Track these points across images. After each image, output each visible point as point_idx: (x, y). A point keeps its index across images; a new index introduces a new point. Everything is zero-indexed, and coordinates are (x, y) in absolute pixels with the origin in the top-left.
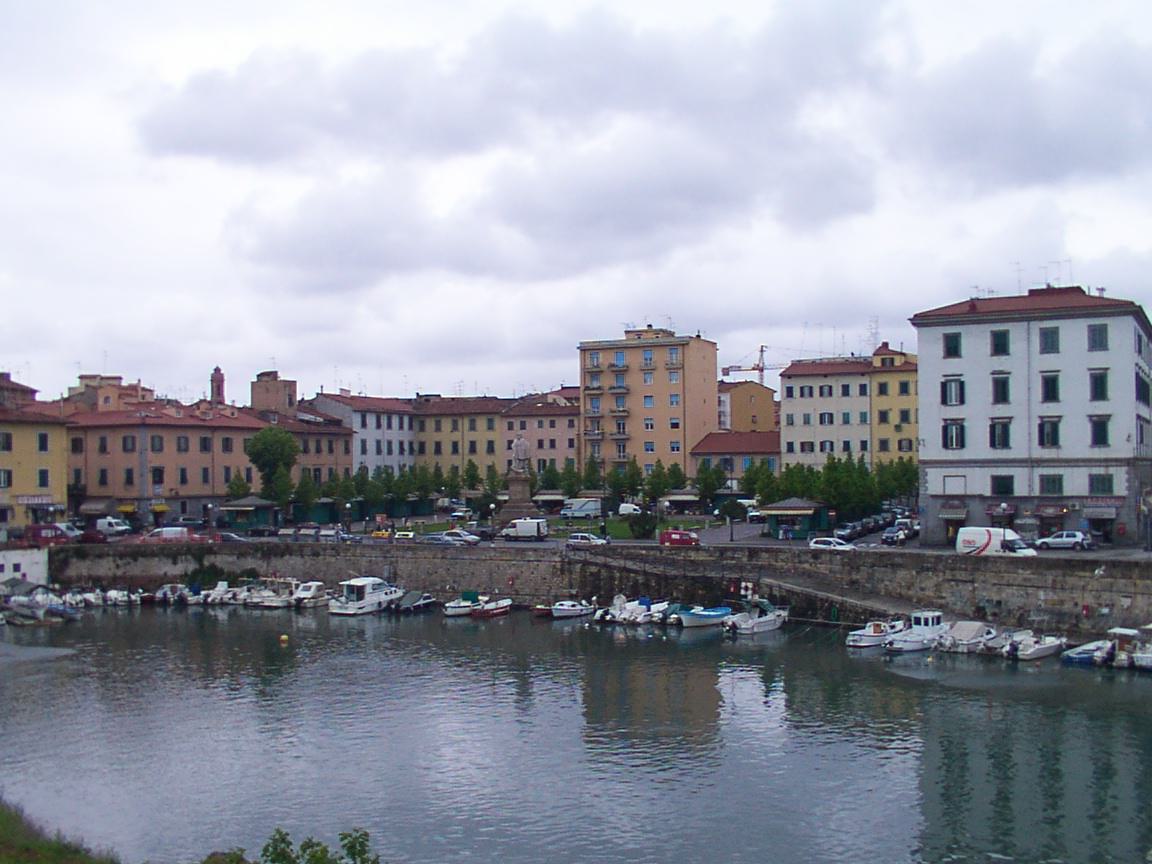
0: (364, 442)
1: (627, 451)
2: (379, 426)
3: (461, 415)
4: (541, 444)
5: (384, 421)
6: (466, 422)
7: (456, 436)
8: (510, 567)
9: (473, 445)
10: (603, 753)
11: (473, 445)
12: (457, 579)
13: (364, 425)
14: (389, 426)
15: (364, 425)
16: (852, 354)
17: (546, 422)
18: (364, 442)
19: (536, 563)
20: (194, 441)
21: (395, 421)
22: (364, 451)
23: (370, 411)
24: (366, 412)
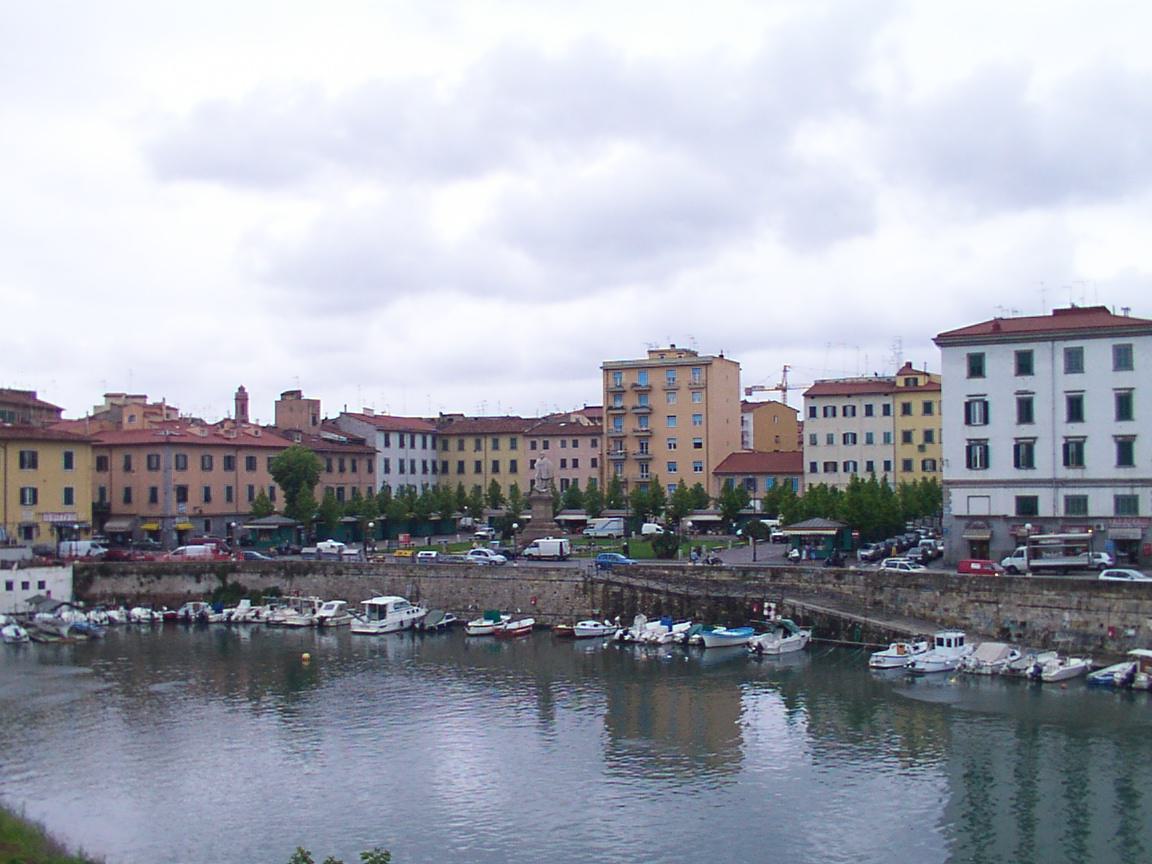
0: (387, 461)
2: (402, 445)
3: (485, 435)
4: (563, 463)
5: (407, 439)
6: (588, 440)
8: (533, 587)
9: (496, 464)
11: (496, 464)
13: (387, 444)
14: (413, 446)
15: (387, 444)
18: (387, 461)
21: (418, 440)
22: (387, 470)
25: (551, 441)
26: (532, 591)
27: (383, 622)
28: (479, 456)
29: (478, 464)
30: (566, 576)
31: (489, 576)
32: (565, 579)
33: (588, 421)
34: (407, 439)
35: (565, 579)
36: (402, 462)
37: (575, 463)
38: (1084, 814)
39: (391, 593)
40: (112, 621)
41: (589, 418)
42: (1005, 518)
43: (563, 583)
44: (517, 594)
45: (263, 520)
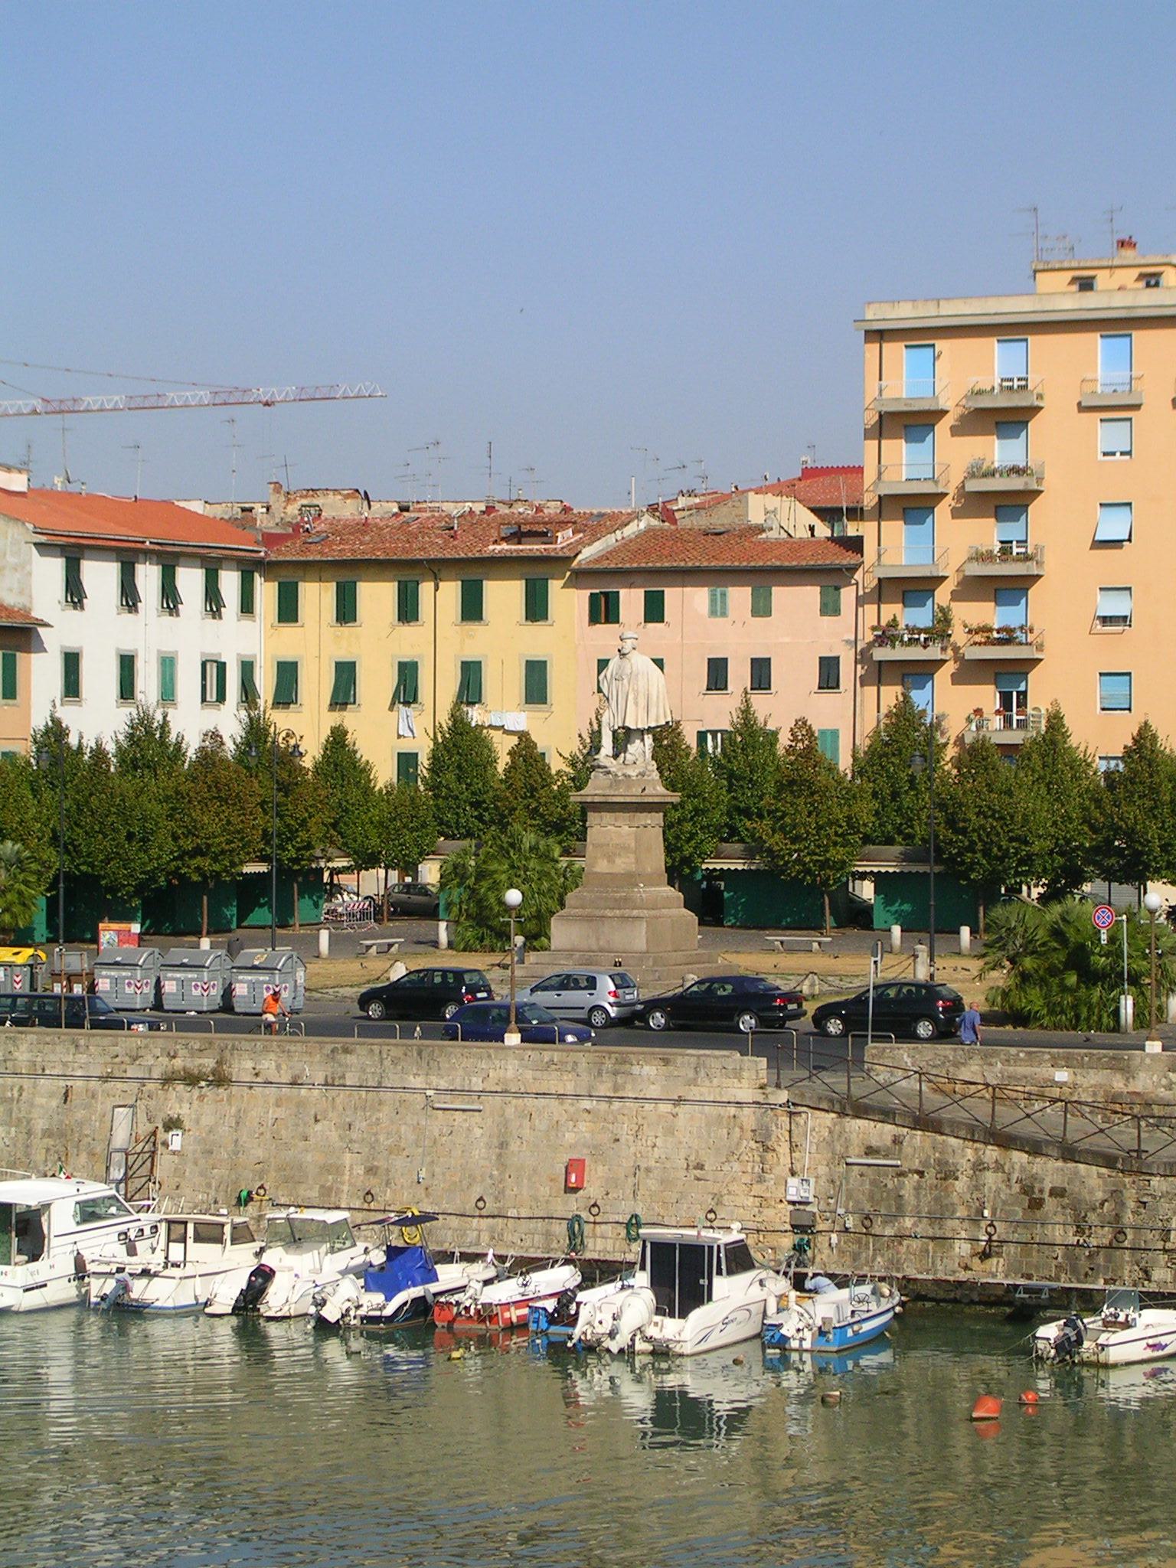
0: (72, 662)
1: (1031, 703)
2: (129, 597)
3: (436, 569)
4: (717, 674)
5: (148, 577)
6: (450, 592)
7: (411, 642)
8: (574, 1120)
9: (346, 675)
10: (15, 1395)
11: (346, 675)
12: (381, 1163)
13: (75, 593)
14: (247, 606)
15: (75, 593)
16: (779, 480)
17: (740, 596)
18: (72, 662)
19: (665, 1108)
20: (632, 600)
21: (190, 580)
22: (72, 688)
23: (148, 555)
24: (136, 552)
25: (672, 596)
26: (570, 1137)
27: (40, 1270)
28: (411, 642)
29: (407, 673)
30: (693, 1082)
31: (417, 1082)
32: (694, 1093)
33: (813, 520)
34: (148, 577)
35: (694, 1093)
36: (127, 663)
37: (761, 673)
38: (1071, 1544)
39: (58, 1166)
40: (160, 1559)
41: (818, 512)
42: (665, 816)
43: (683, 1110)
44: (514, 1146)
45: (593, 968)
